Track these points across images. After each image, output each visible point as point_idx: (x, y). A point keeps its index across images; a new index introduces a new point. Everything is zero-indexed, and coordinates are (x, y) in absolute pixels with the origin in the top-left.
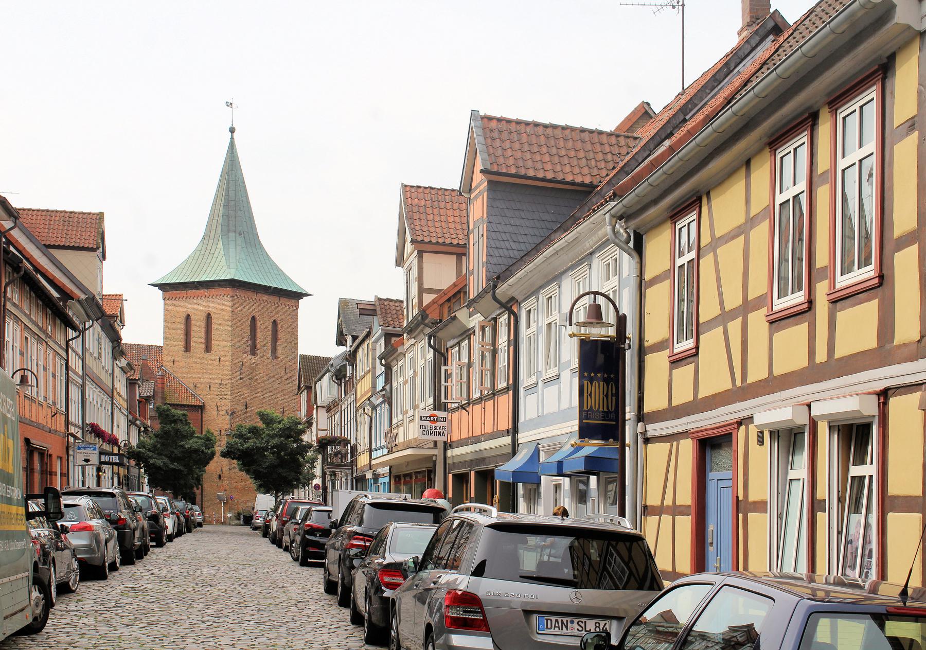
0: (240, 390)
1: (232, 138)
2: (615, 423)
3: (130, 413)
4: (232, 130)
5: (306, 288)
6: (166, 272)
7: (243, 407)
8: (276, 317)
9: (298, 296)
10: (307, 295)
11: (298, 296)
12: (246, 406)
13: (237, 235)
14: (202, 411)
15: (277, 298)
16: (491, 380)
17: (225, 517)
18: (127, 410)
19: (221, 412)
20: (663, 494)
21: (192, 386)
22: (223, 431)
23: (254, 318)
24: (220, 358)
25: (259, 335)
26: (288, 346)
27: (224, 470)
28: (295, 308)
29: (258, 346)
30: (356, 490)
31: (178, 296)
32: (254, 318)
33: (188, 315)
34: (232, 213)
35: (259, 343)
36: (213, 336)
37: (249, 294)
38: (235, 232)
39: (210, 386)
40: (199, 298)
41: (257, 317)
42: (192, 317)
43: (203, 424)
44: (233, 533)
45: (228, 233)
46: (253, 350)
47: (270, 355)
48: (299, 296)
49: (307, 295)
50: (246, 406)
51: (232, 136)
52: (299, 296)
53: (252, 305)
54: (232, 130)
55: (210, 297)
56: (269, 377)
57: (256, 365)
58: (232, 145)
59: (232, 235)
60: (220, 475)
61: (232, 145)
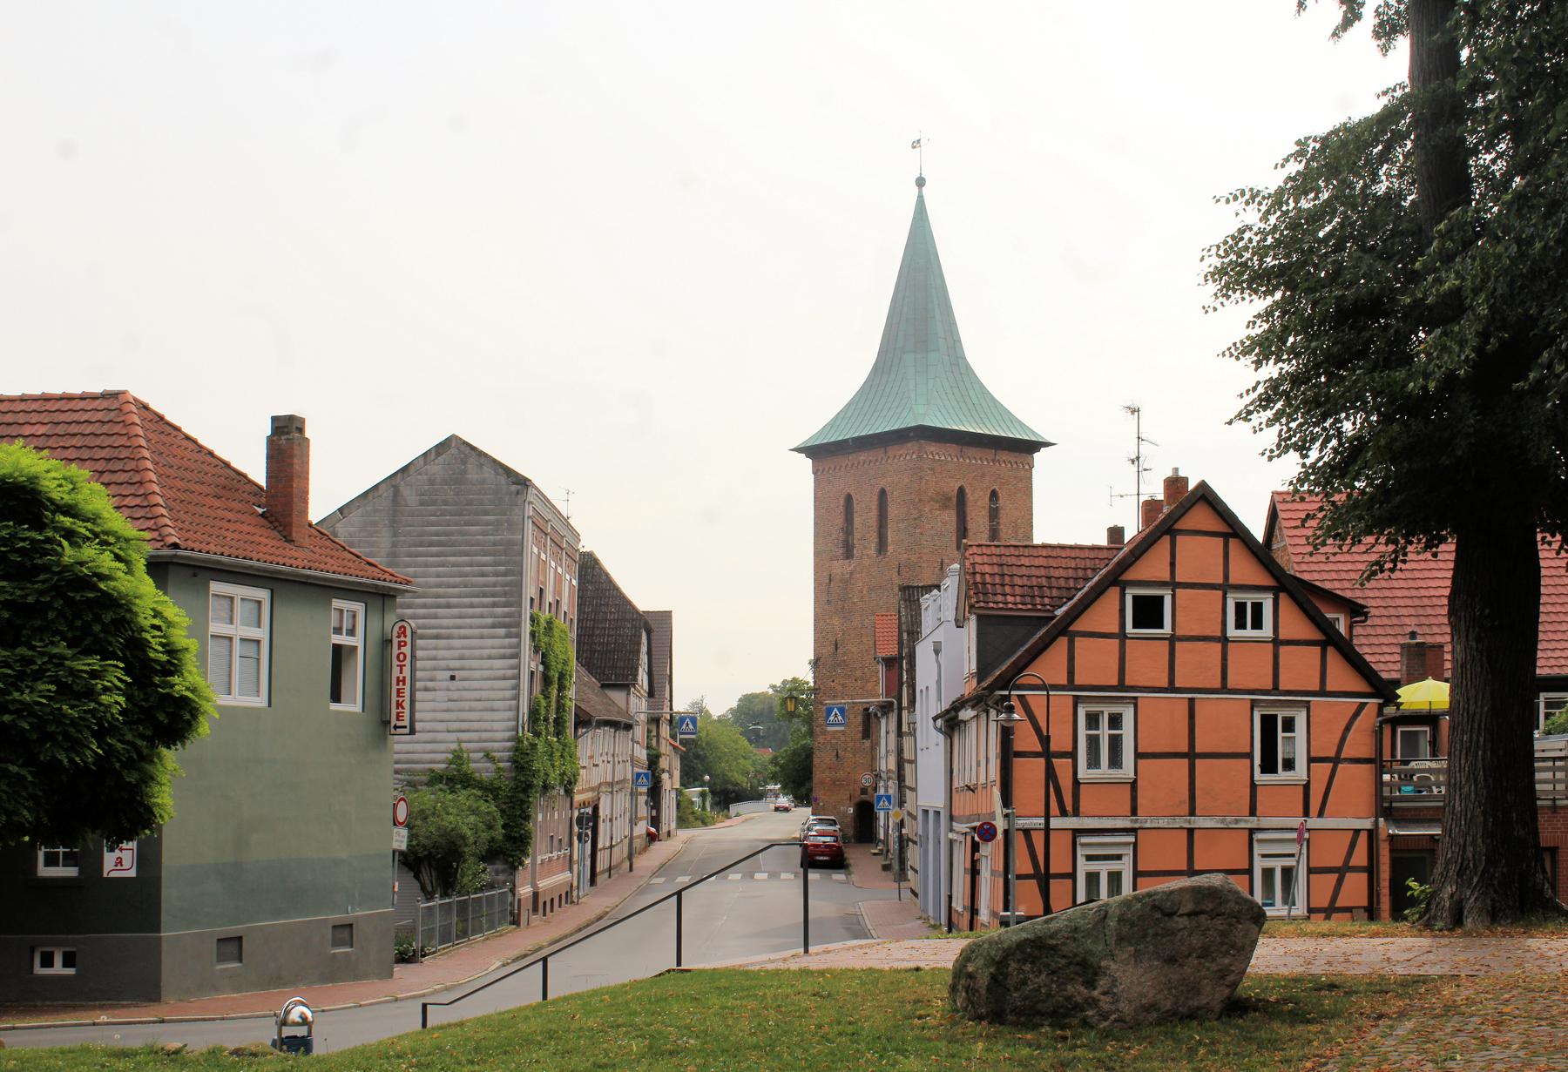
2: (71, 872)
4: (920, 182)
6: (810, 427)
8: (882, 484)
9: (1032, 446)
11: (1032, 446)
15: (883, 450)
16: (1212, 512)
20: (1188, 845)
23: (849, 498)
28: (1027, 467)
30: (1253, 627)
32: (849, 498)
41: (853, 493)
44: (588, 926)
46: (849, 554)
47: (872, 551)
48: (1031, 447)
52: (1031, 447)
53: (954, 470)
54: (920, 182)
58: (921, 200)
61: (921, 200)
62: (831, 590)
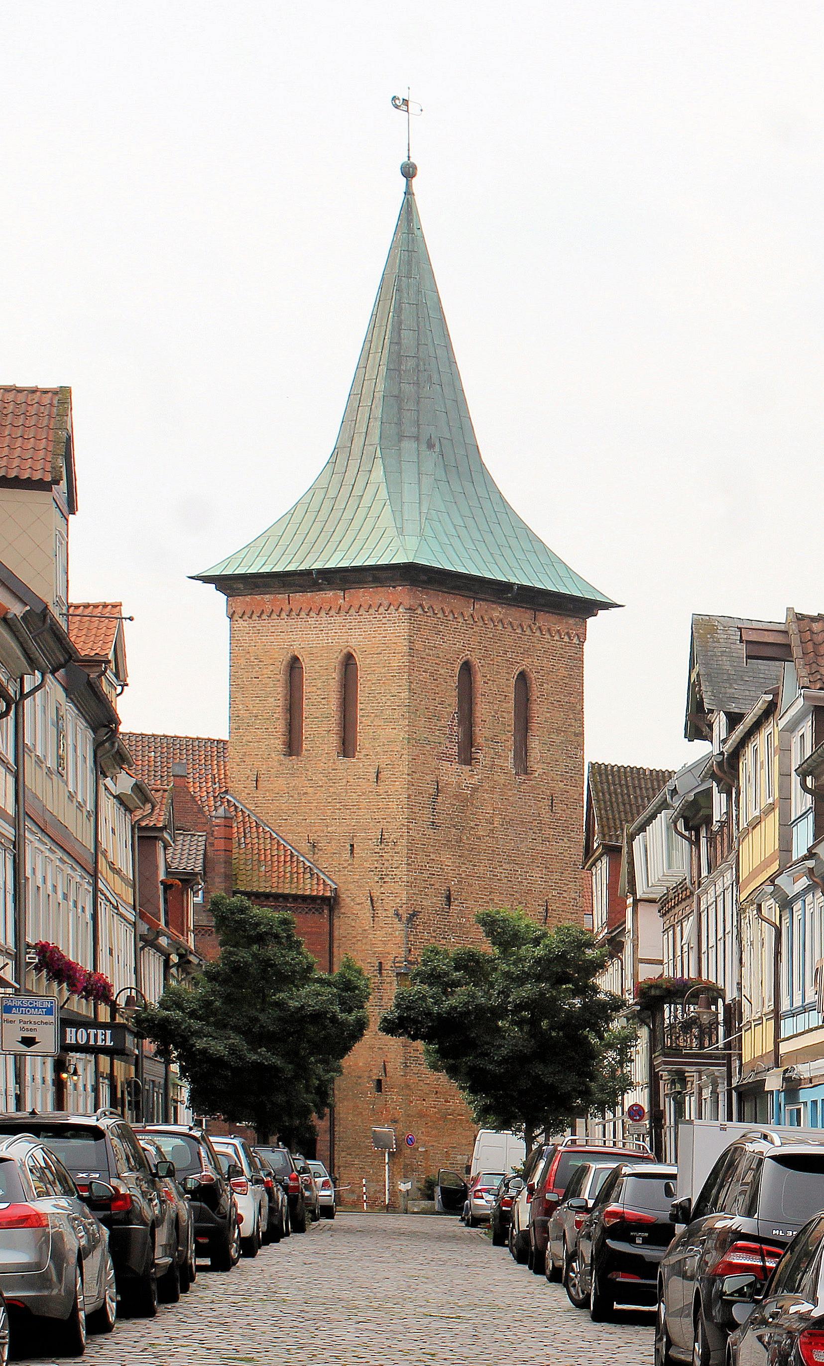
0: (433, 856)
1: (409, 192)
3: (142, 916)
4: (409, 172)
5: (607, 591)
7: (440, 901)
10: (607, 606)
12: (448, 898)
13: (424, 447)
14: (331, 911)
15: (529, 614)
17: (394, 1193)
18: (134, 909)
19: (381, 913)
21: (305, 847)
22: (388, 965)
23: (467, 668)
24: (378, 773)
25: (482, 710)
26: (558, 739)
27: (389, 1067)
29: (480, 740)
31: (268, 607)
32: (467, 668)
33: (295, 660)
34: (408, 389)
35: (482, 733)
36: (359, 713)
37: (455, 602)
38: (417, 439)
39: (352, 846)
40: (323, 614)
41: (476, 663)
42: (306, 663)
43: (335, 945)
45: (400, 441)
49: (607, 606)
50: (448, 898)
51: (409, 186)
54: (409, 172)
55: (352, 611)
56: (507, 823)
57: (475, 789)
58: (408, 212)
59: (408, 446)
60: (379, 1082)
61: (408, 212)
62: (439, 807)
